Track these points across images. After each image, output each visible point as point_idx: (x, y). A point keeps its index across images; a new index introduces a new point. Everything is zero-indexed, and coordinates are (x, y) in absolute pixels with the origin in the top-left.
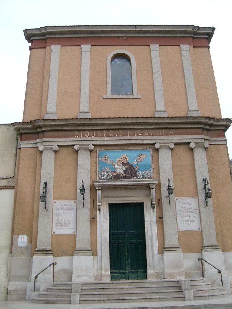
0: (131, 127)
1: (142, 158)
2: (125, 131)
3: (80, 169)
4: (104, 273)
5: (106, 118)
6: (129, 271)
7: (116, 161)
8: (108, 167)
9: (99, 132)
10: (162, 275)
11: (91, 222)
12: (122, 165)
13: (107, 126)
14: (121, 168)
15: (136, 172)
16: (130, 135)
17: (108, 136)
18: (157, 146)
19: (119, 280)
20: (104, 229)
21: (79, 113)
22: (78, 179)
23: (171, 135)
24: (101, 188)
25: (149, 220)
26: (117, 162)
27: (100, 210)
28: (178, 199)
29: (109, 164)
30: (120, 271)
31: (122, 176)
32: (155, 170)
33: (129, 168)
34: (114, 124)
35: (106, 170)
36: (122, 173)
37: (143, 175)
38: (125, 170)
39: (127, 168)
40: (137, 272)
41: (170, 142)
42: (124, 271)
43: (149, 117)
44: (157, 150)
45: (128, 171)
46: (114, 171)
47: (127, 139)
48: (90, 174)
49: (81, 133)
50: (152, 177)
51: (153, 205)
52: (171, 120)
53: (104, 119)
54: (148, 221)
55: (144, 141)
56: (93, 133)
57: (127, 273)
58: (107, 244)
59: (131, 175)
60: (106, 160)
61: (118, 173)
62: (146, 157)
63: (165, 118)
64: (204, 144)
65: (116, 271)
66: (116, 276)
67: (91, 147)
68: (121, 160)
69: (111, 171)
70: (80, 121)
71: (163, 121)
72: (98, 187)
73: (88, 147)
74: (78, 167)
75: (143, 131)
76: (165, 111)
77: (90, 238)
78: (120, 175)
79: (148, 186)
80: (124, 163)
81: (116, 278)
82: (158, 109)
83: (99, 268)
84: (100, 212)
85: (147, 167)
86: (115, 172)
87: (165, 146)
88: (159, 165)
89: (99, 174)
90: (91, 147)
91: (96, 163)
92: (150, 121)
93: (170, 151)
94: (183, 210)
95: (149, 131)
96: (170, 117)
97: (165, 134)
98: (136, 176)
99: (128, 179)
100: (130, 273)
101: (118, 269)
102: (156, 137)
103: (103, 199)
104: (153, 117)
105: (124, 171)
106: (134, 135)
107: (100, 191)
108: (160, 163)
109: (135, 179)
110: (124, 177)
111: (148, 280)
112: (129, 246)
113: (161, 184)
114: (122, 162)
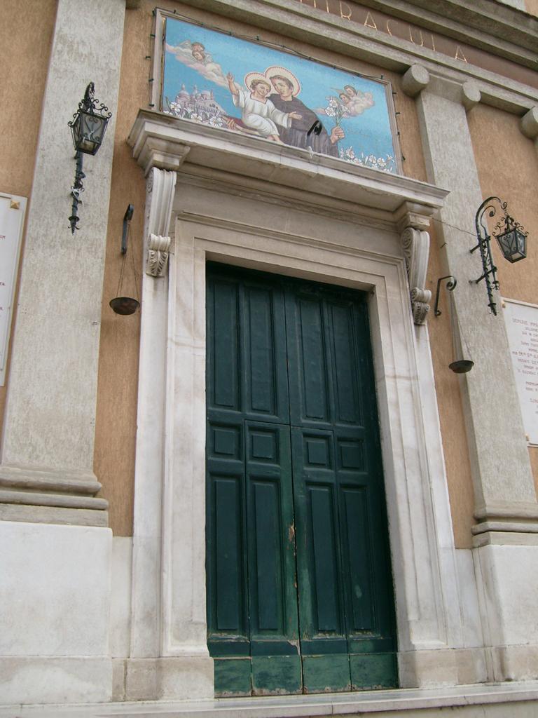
1: (355, 103)
3: (66, 56)
4: (171, 648)
6: (306, 639)
8: (209, 93)
10: (479, 663)
11: (107, 329)
12: (270, 104)
19: (253, 695)
20: (177, 381)
24: (177, 163)
25: (402, 370)
26: (249, 84)
27: (156, 277)
28: (508, 305)
30: (255, 638)
38: (285, 124)
39: (294, 120)
40: (345, 647)
42: (278, 638)
51: (423, 305)
54: (400, 377)
57: (290, 650)
58: (195, 468)
61: (256, 130)
65: (234, 637)
66: (231, 670)
72: (167, 152)
74: (57, 45)
77: (94, 415)
81: (232, 680)
83: (138, 615)
84: (156, 288)
91: (149, 58)
94: (529, 355)
100: (309, 649)
101: (244, 628)
103: (178, 222)
105: (279, 127)
107: (174, 176)
111: (413, 685)
112: (301, 498)
114: (274, 91)
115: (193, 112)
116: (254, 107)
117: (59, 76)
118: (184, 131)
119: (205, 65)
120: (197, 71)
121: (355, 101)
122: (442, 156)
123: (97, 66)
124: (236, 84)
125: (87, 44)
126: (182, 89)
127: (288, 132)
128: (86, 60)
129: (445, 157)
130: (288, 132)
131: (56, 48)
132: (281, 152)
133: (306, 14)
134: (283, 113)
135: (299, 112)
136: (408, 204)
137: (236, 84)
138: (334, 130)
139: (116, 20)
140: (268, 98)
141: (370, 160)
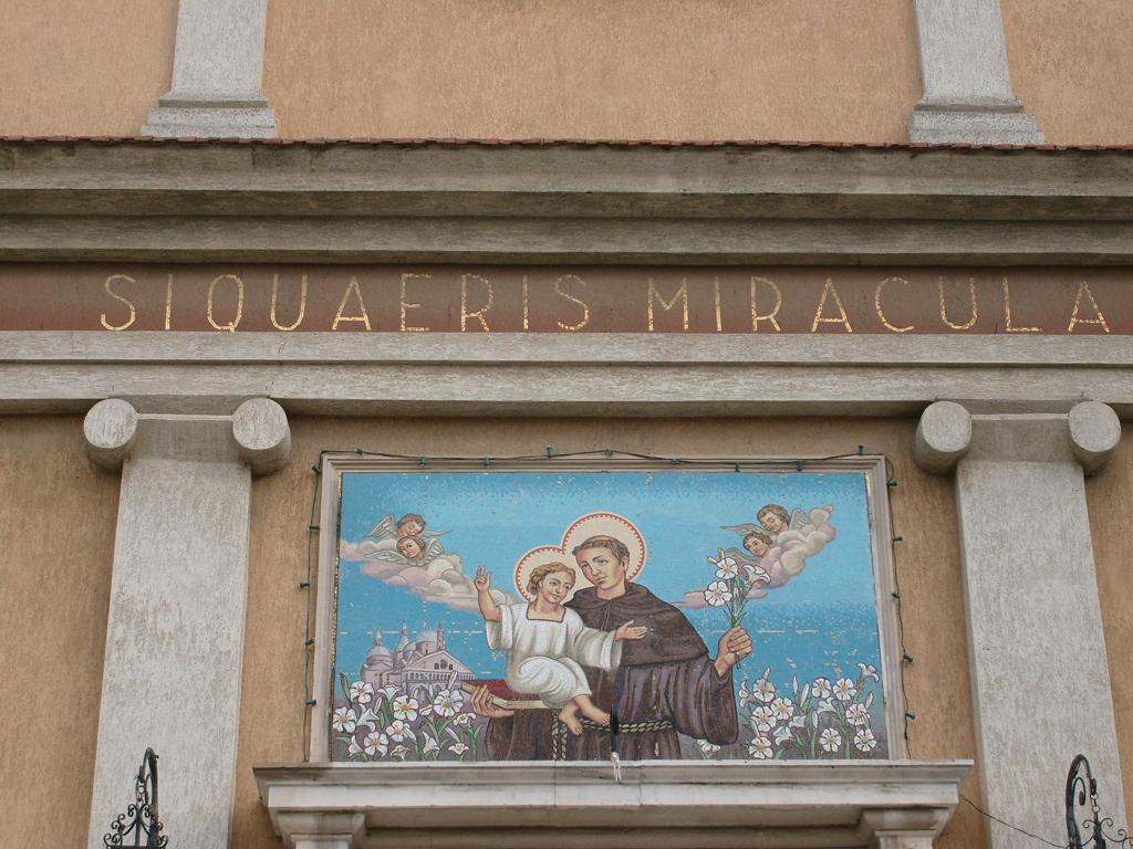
0: (675, 244)
2: (614, 288)
3: (132, 651)
5: (428, 144)
7: (513, 575)
8: (432, 636)
9: (354, 283)
12: (573, 619)
13: (432, 228)
14: (571, 652)
15: (722, 691)
16: (668, 324)
17: (445, 323)
18: (943, 431)
21: (163, 104)
22: (102, 750)
23: (1079, 330)
26: (525, 581)
29: (441, 607)
31: (574, 725)
32: (922, 682)
33: (655, 645)
34: (511, 210)
35: (413, 667)
36: (573, 701)
37: (799, 722)
39: (628, 645)
41: (1076, 395)
43: (862, 147)
44: (943, 474)
45: (640, 677)
46: (486, 674)
47: (631, 355)
48: (232, 704)
49: (170, 290)
50: (894, 743)
52: (1080, 177)
53: (405, 156)
55: (798, 382)
56: (295, 297)
59: (672, 719)
60: (412, 560)
61: (536, 697)
62: (832, 538)
63: (1018, 160)
64: (1077, 414)
67: (263, 430)
68: (570, 561)
69: (459, 668)
70: (158, 168)
71: (997, 189)
73: (230, 424)
74: (116, 630)
75: (801, 286)
76: (1018, 109)
78: (551, 715)
79: (845, 839)
80: (602, 595)
82: (939, 87)
85: (830, 641)
86: (500, 688)
87: (1024, 434)
88: (962, 626)
89: (333, 706)
90: (263, 430)
91: (307, 587)
92: (872, 186)
93: (1071, 485)
95: (855, 285)
96: (1073, 151)
97: (1012, 326)
98: (727, 732)
99: (637, 756)
102: (927, 349)
104: (895, 148)
105: (593, 674)
106: (702, 325)
108: (975, 603)
109: (716, 756)
110: (599, 741)
113: (995, 827)
114: (582, 583)
115: (397, 695)
116: (534, 639)
117: (121, 700)
118: (347, 786)
119: (425, 566)
120: (408, 587)
121: (782, 545)
122: (1005, 632)
123: (193, 654)
124: (494, 592)
125: (174, 607)
126: (376, 644)
127: (611, 679)
128: (173, 647)
129: (1012, 634)
130: (611, 679)
131: (113, 635)
132: (555, 777)
133: (657, 358)
134: (603, 634)
135: (638, 618)
136: (868, 817)
137: (494, 592)
138: (726, 638)
139: (231, 529)
140: (567, 605)
141: (815, 693)
